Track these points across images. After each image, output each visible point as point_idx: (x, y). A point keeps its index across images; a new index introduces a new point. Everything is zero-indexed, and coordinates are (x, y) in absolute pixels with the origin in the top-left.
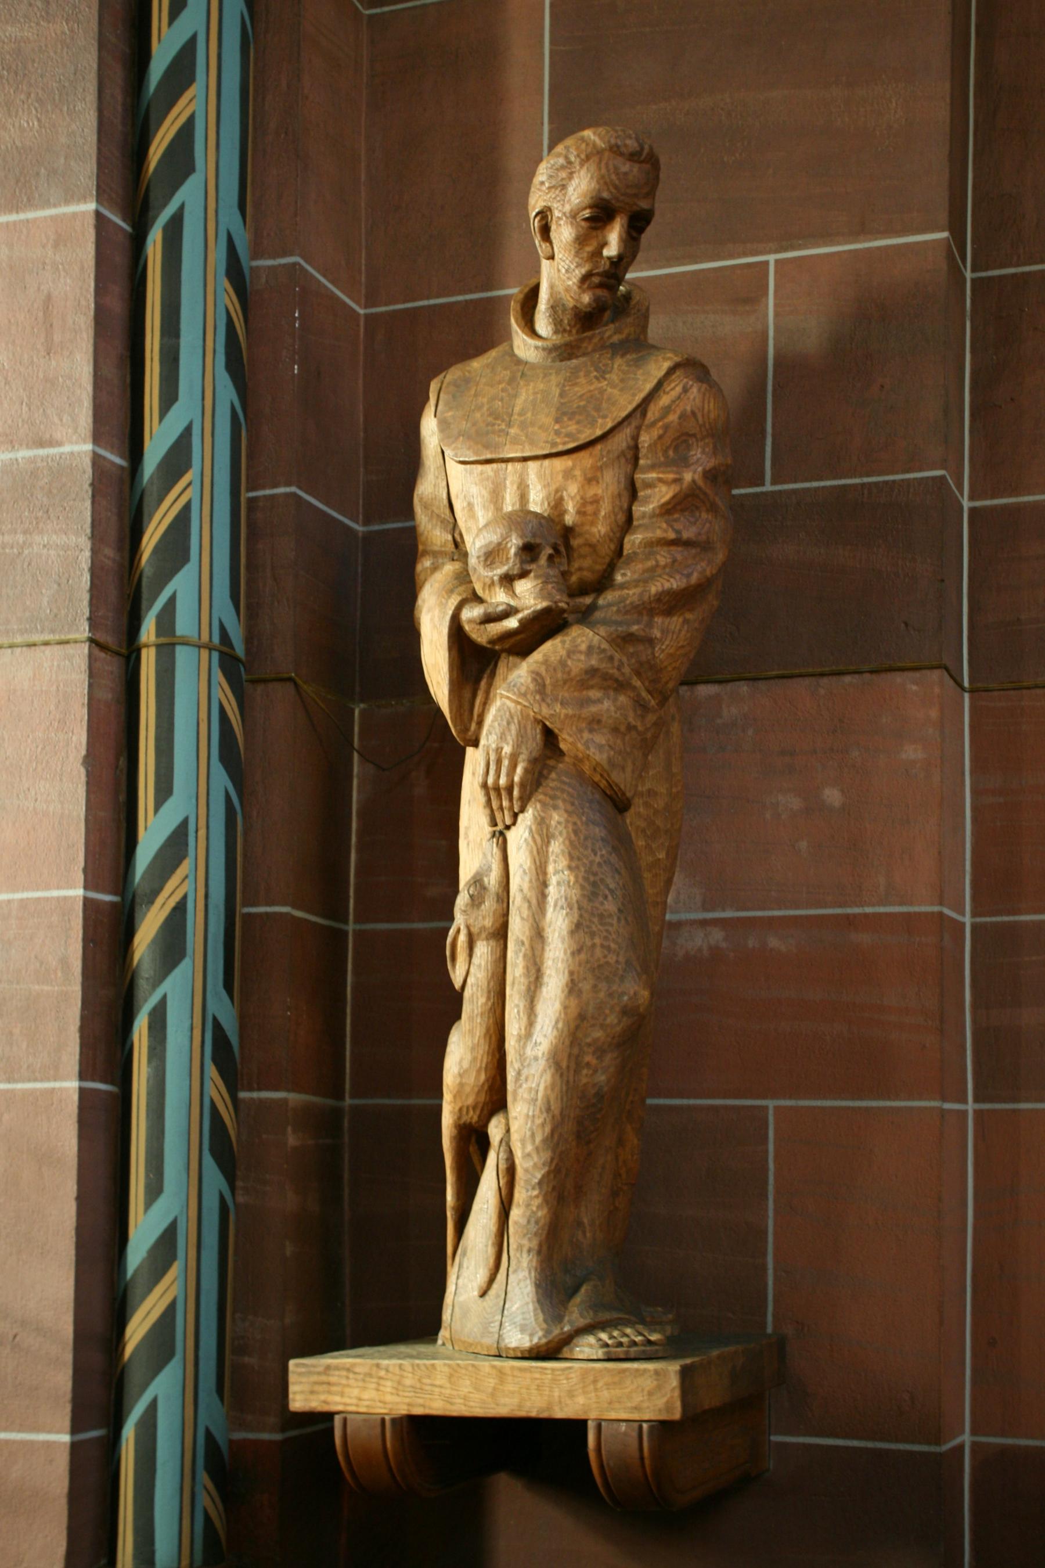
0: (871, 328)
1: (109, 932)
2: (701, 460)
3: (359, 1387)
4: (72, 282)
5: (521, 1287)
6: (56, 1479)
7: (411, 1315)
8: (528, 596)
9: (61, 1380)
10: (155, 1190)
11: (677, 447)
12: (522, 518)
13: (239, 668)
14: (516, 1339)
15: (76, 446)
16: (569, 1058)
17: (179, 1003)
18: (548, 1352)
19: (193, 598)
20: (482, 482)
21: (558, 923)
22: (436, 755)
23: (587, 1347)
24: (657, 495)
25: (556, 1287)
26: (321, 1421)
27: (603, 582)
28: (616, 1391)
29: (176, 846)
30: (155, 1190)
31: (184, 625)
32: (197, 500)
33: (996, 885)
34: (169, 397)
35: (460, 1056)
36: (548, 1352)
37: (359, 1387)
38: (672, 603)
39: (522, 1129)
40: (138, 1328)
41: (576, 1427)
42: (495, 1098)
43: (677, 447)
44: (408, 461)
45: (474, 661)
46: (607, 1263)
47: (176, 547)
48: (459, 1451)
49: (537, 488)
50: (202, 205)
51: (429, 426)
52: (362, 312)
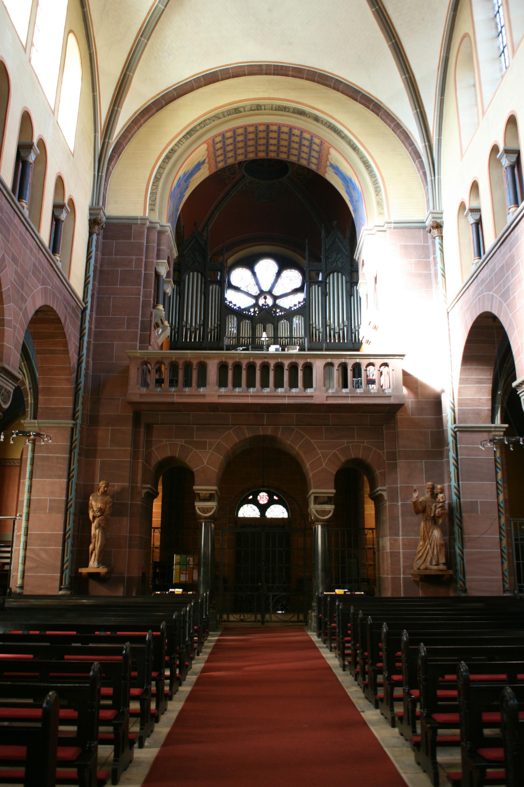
0: (123, 490)
1: (64, 535)
2: (111, 504)
3: (84, 570)
4: (64, 486)
5: (96, 563)
6: (59, 578)
7: (87, 565)
8: (99, 514)
9: (59, 570)
10: (67, 556)
11: (109, 503)
12: (98, 508)
13: (74, 515)
14: (96, 567)
15: (64, 498)
16: (100, 547)
17: (69, 541)
18: (98, 567)
19: (72, 510)
20: (95, 504)
21: (100, 537)
22: (90, 523)
23: (101, 567)
24: (108, 507)
25: (99, 563)
26: (81, 573)
27: (104, 512)
28: (103, 570)
29: (69, 530)
30: (67, 556)
31: (72, 512)
32: (72, 502)
33: (131, 532)
34: (71, 494)
35: (91, 547)
36: (98, 567)
37: (84, 570)
38: (108, 514)
39: (97, 551)
40: (65, 567)
41: (100, 573)
42: (94, 549)
43: (109, 503)
44: (89, 500)
45: (94, 518)
46: (101, 562)
47: (71, 506)
48: (92, 575)
49: (99, 505)
50: (74, 480)
51: (91, 498)
52: (12, 304)
